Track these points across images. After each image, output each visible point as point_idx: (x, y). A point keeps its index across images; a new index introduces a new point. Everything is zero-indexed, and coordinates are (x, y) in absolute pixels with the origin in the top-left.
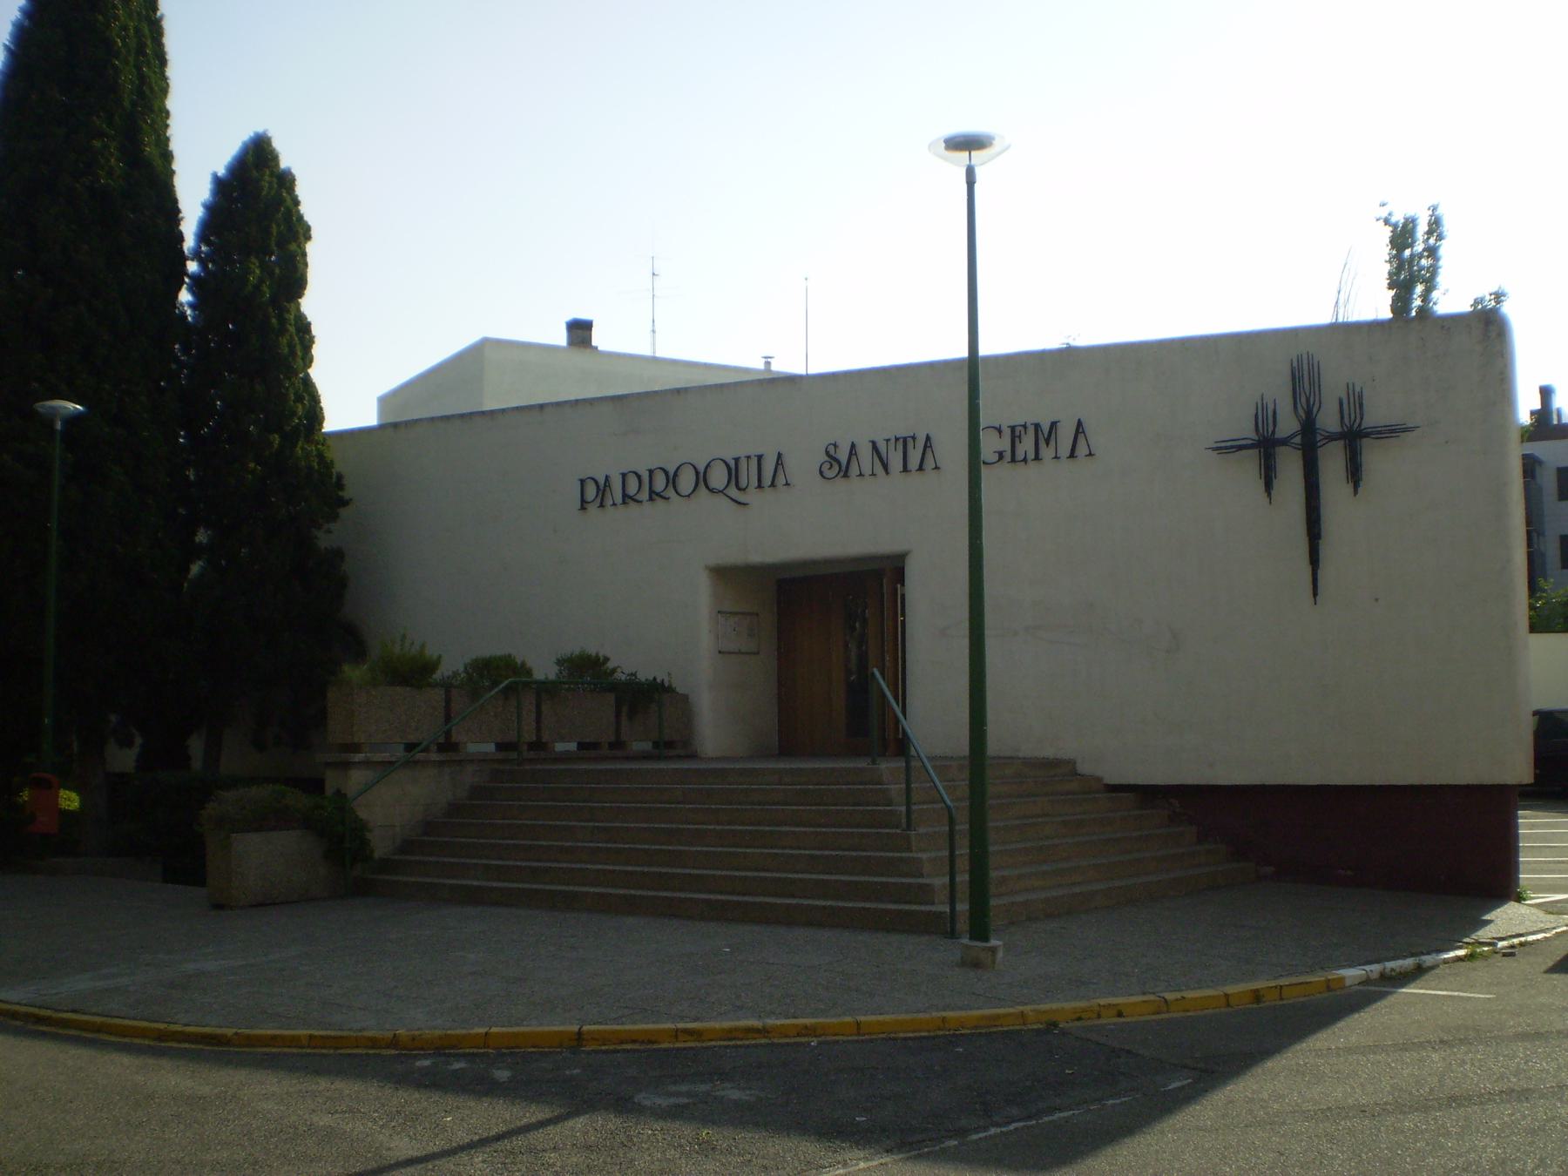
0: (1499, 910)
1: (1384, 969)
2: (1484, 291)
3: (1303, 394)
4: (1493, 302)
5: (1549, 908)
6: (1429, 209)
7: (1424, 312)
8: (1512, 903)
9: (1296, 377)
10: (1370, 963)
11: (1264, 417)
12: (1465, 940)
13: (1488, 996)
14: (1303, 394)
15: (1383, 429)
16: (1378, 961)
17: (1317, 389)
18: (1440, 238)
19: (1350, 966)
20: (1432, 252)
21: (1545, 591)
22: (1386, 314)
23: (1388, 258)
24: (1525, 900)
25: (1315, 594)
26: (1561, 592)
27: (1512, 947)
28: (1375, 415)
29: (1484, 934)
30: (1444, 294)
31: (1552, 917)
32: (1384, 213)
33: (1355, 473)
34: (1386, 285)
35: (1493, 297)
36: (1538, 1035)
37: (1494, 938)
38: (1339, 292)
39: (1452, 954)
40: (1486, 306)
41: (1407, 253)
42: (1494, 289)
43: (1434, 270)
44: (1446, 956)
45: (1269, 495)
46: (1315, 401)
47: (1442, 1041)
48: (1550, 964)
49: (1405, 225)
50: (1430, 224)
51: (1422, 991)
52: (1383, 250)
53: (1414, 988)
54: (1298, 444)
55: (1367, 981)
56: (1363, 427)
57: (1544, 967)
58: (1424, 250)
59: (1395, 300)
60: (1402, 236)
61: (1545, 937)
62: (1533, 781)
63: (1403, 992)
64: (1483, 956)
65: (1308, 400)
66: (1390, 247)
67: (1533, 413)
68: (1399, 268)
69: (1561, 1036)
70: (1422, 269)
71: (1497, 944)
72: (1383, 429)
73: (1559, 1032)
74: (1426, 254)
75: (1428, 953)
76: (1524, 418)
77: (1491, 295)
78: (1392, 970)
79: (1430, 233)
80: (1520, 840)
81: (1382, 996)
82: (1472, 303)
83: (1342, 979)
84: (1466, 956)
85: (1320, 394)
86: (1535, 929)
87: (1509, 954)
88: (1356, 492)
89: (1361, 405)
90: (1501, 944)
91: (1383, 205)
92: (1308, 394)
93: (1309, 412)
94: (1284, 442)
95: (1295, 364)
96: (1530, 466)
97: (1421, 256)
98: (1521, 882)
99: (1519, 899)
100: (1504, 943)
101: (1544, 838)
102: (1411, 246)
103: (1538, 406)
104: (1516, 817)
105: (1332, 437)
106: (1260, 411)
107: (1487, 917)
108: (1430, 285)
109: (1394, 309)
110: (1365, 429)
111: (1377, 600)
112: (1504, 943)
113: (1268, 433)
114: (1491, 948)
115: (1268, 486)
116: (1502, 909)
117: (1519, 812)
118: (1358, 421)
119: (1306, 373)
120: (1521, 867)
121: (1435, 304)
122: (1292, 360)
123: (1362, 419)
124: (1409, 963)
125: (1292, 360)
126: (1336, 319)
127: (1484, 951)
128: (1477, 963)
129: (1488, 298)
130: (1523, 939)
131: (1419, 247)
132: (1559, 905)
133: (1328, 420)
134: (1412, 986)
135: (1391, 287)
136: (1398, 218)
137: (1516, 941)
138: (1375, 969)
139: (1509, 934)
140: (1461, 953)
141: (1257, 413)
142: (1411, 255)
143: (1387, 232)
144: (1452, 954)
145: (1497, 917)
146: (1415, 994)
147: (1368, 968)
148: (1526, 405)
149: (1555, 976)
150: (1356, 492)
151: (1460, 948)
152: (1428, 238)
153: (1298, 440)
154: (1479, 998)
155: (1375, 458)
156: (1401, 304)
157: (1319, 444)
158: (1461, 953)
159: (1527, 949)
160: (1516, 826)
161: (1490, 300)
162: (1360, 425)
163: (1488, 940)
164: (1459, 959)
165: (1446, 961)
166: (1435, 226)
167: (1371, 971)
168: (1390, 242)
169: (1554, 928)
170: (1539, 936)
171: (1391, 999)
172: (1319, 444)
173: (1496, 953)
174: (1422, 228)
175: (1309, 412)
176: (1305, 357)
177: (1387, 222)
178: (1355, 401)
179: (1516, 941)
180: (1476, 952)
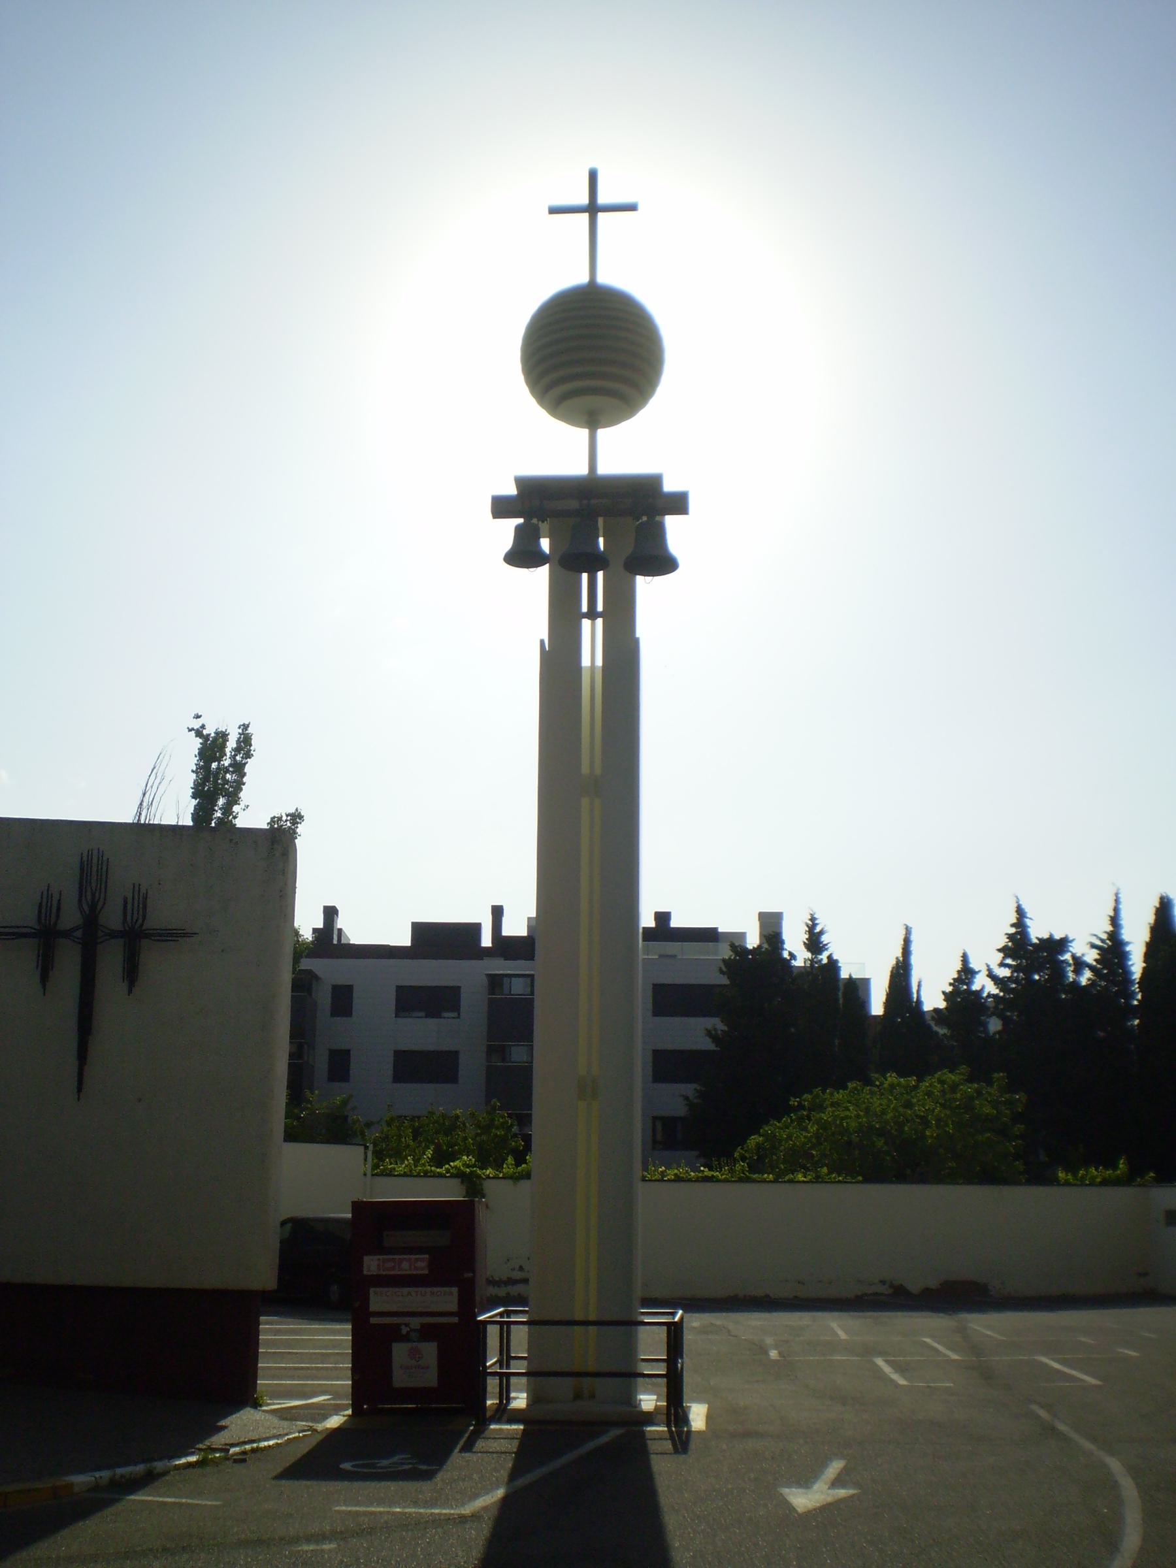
0: (234, 1416)
1: (114, 1475)
2: (282, 810)
3: (89, 889)
4: (288, 823)
5: (286, 1415)
6: (239, 728)
7: (226, 824)
8: (249, 1409)
9: (85, 868)
10: (99, 1469)
11: (48, 907)
12: (197, 1446)
13: (214, 1503)
14: (89, 889)
15: (164, 932)
16: (109, 1467)
17: (103, 886)
18: (248, 755)
19: (80, 1472)
20: (239, 768)
21: (310, 1102)
22: (188, 822)
23: (194, 769)
24: (261, 1406)
25: (80, 1089)
26: (325, 1104)
27: (244, 1453)
28: (161, 915)
29: (218, 1440)
30: (244, 810)
31: (285, 1424)
32: (196, 724)
33: (131, 973)
34: (191, 794)
35: (289, 818)
36: (260, 1542)
37: (226, 1444)
38: (144, 794)
39: (183, 1461)
40: (283, 825)
41: (214, 765)
42: (292, 811)
43: (239, 785)
44: (177, 1463)
45: (44, 986)
46: (100, 898)
47: (165, 1549)
48: (279, 1470)
49: (215, 739)
50: (238, 742)
51: (150, 1498)
52: (190, 760)
53: (143, 1495)
54: (78, 938)
55: (96, 1488)
56: (144, 928)
57: (274, 1474)
58: (230, 765)
59: (198, 808)
60: (211, 747)
61: (277, 1444)
62: (276, 1287)
63: (1094, 1377)
64: (215, 1462)
65: (93, 895)
66: (198, 758)
67: (315, 930)
68: (205, 779)
69: (283, 1542)
70: (227, 782)
71: (229, 1450)
72: (164, 932)
73: (281, 1539)
74: (231, 769)
75: (161, 1459)
76: (307, 934)
77: (287, 816)
78: (122, 1476)
79: (237, 750)
80: (260, 1346)
81: (112, 1502)
82: (269, 821)
83: (72, 1485)
84: (197, 1462)
85: (106, 892)
86: (268, 1435)
87: (241, 1459)
88: (130, 992)
89: (145, 908)
90: (233, 1450)
91: (198, 717)
92: (93, 889)
93: (93, 906)
94: (67, 934)
95: (85, 859)
96: (303, 984)
97: (227, 771)
98: (258, 1388)
99: (256, 1405)
100: (237, 1449)
101: (288, 1344)
102: (219, 760)
103: (320, 925)
104: (258, 1323)
105: (113, 935)
106: (45, 900)
107: (223, 1423)
108: (233, 799)
109: (195, 816)
110: (147, 929)
111: (140, 1100)
112: (237, 1449)
113: (50, 921)
114: (222, 1454)
115: (44, 978)
116: (238, 1415)
117: (261, 1318)
118: (140, 921)
119: (94, 869)
120: (260, 1373)
121: (235, 817)
122: (82, 854)
123: (143, 921)
124: (140, 1468)
125: (82, 854)
126: (178, 822)
127: (215, 1457)
128: (208, 1469)
129: (284, 818)
130: (255, 1445)
131: (226, 762)
132: (294, 1411)
133: (112, 917)
134: (140, 1493)
135: (194, 796)
136: (210, 730)
137: (248, 1447)
138: (105, 1474)
139: (241, 1440)
140: (193, 1459)
141: (42, 901)
142: (217, 769)
143: (197, 743)
144: (183, 1461)
145: (232, 1423)
146: (143, 1501)
147: (97, 1474)
148: (647, 920)
149: (283, 1482)
150: (130, 992)
151: (192, 1454)
152: (236, 755)
153: (79, 933)
154: (206, 1505)
155: (153, 960)
156: (202, 813)
157: (99, 941)
158: (193, 1459)
159: (258, 1455)
160: (257, 1332)
161: (286, 821)
162: (142, 925)
163: (220, 1447)
164: (190, 1465)
165: (177, 1467)
166: (245, 741)
167: (101, 1477)
168: (199, 754)
169: (287, 1434)
170: (271, 1443)
171: (119, 1507)
172: (99, 941)
173: (228, 1459)
174: (231, 744)
175: (93, 906)
176: (95, 853)
177: (199, 733)
178: (139, 901)
179: (248, 1447)
180: (207, 1458)
